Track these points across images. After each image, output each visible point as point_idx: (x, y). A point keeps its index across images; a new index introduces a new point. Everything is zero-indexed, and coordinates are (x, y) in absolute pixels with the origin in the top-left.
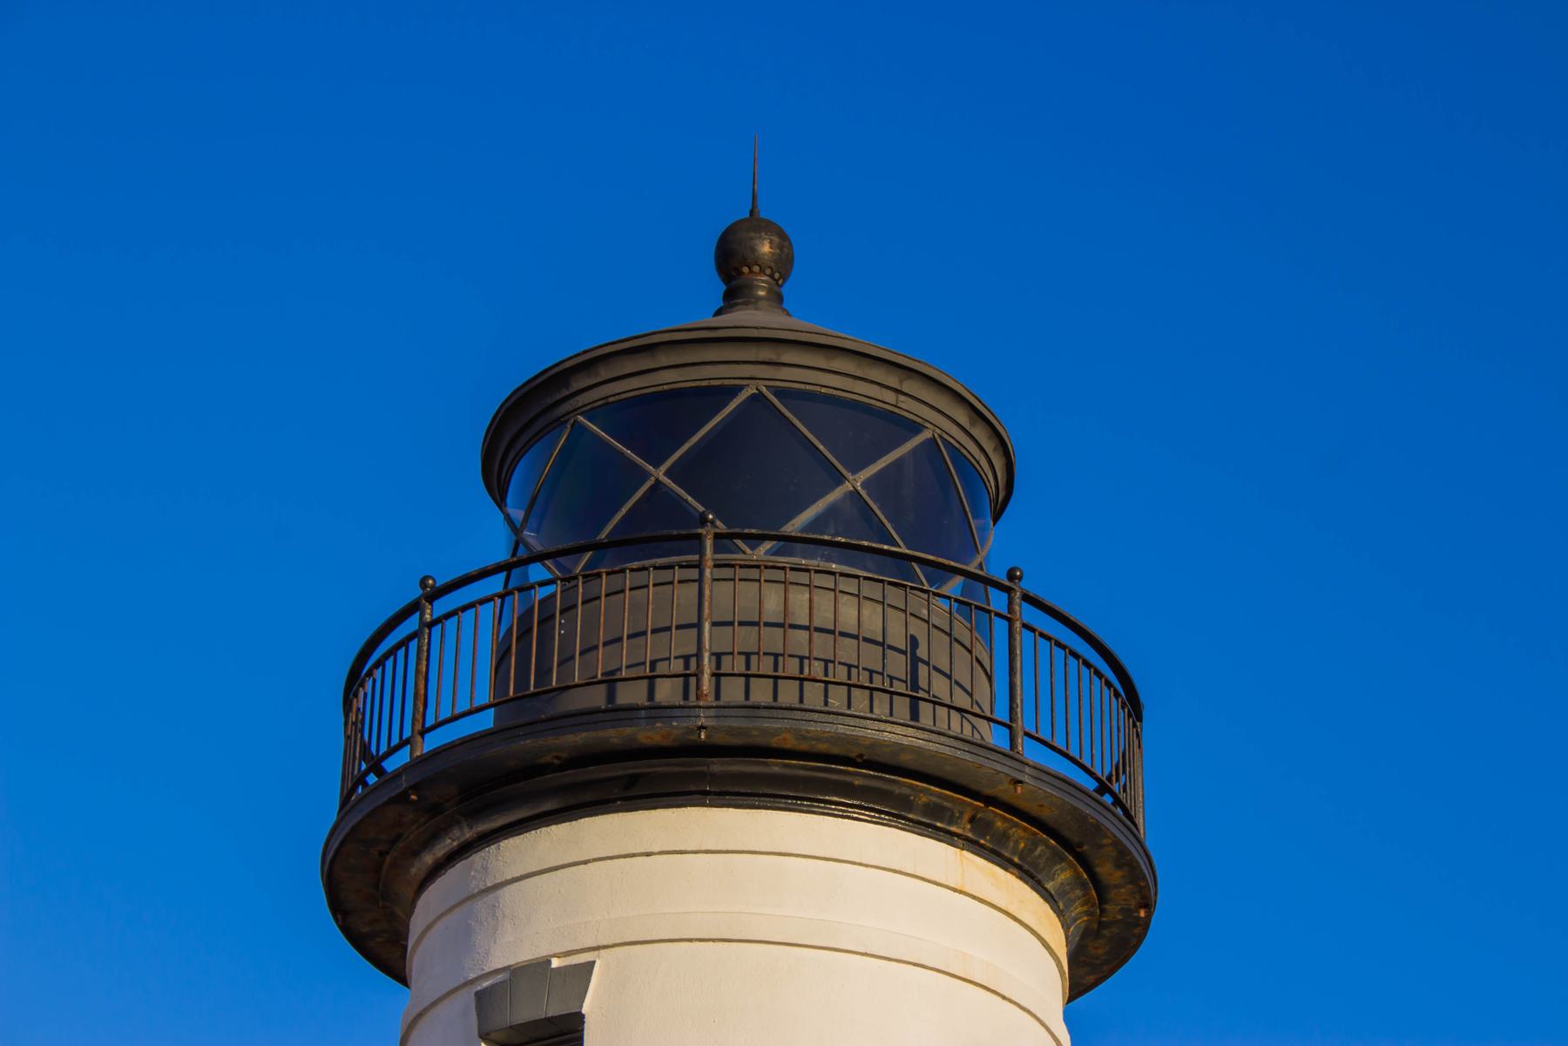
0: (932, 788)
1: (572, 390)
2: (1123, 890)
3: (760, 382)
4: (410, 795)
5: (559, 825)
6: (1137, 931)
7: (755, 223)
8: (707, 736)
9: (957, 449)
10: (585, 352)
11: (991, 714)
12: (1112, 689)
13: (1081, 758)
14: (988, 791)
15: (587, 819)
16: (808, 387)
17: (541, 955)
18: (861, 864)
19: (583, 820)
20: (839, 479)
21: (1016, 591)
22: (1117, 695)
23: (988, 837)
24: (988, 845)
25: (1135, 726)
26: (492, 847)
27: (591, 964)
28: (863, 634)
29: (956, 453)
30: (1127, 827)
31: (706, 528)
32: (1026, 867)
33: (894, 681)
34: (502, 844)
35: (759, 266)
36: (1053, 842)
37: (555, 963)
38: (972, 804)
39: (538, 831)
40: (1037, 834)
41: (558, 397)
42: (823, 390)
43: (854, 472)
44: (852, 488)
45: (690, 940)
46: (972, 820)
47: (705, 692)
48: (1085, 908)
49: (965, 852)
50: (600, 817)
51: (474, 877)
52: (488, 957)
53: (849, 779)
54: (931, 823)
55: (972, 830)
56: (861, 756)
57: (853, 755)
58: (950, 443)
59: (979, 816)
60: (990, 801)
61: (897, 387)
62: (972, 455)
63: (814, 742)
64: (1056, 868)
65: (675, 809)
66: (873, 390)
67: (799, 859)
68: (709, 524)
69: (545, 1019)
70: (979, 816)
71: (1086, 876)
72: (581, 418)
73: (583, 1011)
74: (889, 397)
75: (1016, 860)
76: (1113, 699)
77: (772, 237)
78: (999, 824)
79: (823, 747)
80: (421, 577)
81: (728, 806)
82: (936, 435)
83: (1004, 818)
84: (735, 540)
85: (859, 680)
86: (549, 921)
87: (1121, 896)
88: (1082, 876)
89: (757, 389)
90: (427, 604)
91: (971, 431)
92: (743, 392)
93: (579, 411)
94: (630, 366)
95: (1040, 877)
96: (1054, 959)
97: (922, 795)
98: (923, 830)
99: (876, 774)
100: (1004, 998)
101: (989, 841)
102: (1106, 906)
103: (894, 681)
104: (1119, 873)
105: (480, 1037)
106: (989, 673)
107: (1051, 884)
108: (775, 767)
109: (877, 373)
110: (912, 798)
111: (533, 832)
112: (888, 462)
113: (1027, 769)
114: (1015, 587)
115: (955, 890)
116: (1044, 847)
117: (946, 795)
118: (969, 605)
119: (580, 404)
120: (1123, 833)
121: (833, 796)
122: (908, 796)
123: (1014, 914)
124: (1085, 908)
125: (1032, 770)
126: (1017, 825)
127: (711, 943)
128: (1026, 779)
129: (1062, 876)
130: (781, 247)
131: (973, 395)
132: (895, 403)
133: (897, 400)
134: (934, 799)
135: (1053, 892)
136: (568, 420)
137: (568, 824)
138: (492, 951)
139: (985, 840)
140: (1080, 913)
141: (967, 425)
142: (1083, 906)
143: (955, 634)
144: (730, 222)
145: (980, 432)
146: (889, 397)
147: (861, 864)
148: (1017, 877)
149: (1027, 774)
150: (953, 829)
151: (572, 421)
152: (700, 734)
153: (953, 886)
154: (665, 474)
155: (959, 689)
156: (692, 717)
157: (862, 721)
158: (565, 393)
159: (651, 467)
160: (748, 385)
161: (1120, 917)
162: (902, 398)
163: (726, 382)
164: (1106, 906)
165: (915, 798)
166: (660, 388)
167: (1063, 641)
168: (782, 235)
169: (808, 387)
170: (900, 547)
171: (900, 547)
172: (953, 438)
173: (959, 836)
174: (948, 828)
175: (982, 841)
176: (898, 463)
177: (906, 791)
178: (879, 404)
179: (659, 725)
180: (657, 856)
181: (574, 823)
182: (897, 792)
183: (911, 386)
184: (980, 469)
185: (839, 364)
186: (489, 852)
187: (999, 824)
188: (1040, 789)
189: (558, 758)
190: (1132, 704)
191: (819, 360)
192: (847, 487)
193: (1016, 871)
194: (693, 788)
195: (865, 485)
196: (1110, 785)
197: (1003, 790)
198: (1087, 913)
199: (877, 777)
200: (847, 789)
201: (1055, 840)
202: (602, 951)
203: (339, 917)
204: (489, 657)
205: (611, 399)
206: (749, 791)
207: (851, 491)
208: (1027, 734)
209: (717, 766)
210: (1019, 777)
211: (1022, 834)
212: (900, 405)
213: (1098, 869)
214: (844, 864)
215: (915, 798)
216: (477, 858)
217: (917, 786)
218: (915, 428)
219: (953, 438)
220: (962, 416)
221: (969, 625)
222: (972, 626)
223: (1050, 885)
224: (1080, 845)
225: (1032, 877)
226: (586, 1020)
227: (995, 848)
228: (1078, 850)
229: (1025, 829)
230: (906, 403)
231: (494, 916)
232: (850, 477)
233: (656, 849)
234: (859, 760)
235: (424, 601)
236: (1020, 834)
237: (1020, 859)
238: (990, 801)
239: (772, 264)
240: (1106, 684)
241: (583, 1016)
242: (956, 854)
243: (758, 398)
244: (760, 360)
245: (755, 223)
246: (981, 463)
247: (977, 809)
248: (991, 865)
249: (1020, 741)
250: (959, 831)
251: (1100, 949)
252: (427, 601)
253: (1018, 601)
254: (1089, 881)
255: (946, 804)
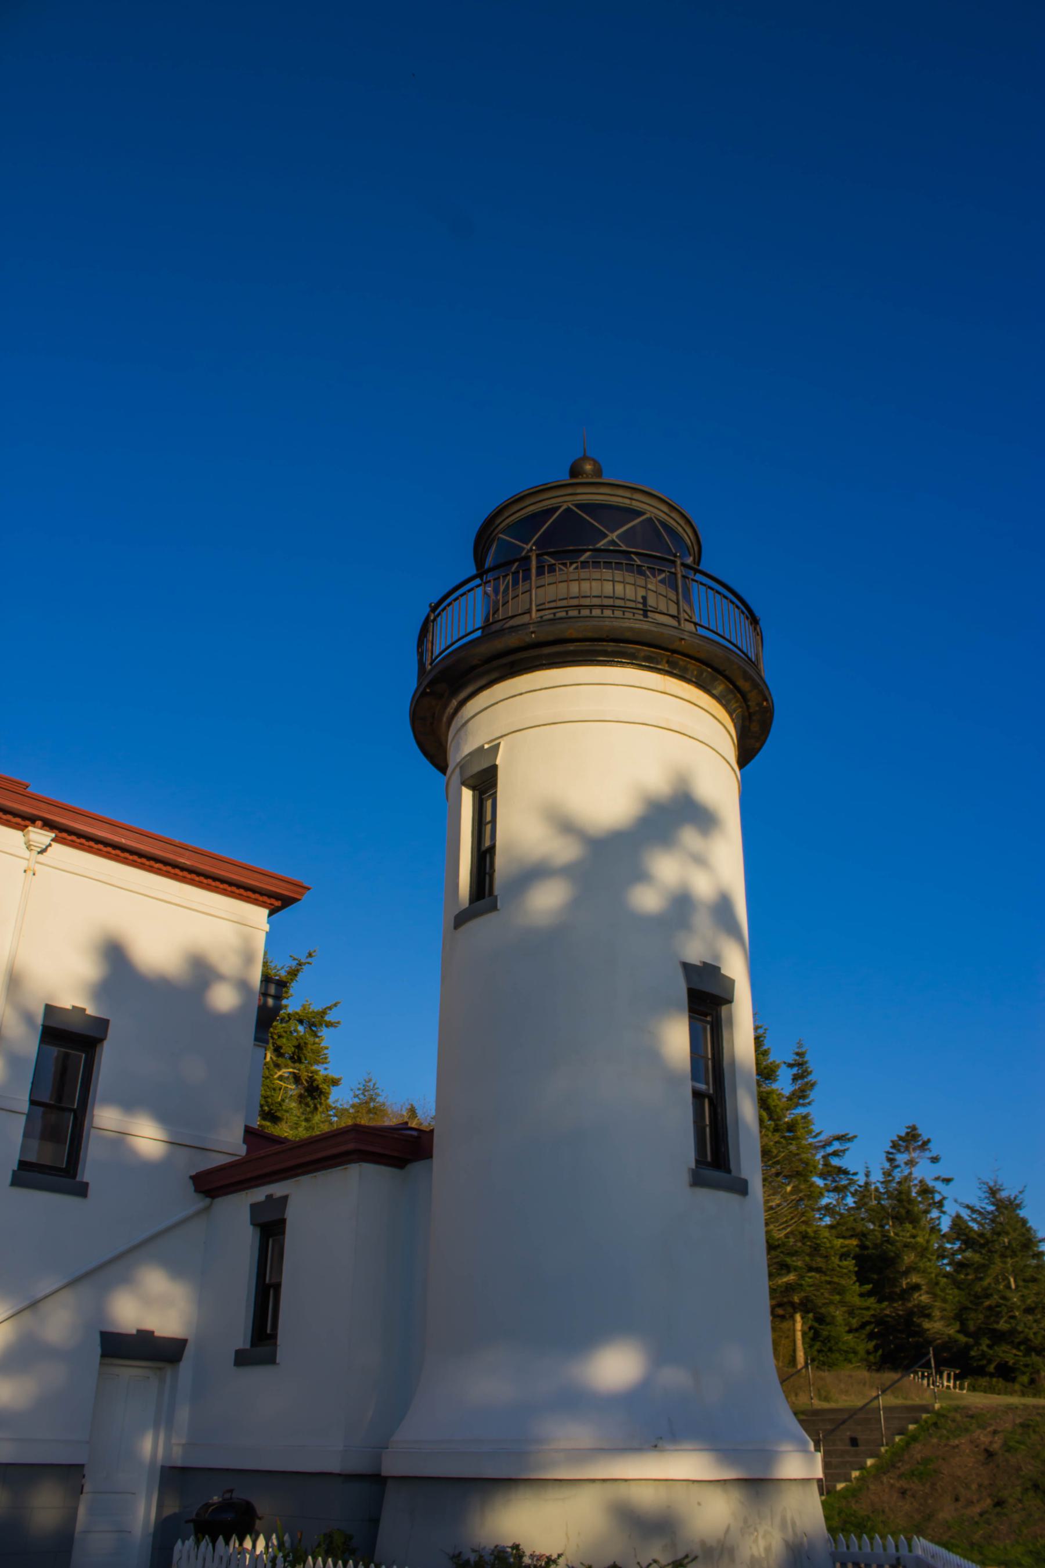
6: (768, 714)
8: (535, 636)
14: (671, 647)
20: (605, 536)
22: (747, 618)
25: (755, 629)
27: (499, 744)
28: (616, 595)
29: (665, 525)
32: (700, 683)
37: (486, 746)
48: (737, 704)
53: (605, 648)
54: (650, 664)
55: (669, 667)
56: (607, 636)
66: (620, 499)
72: (500, 535)
74: (628, 501)
75: (694, 680)
83: (682, 659)
87: (753, 696)
94: (516, 508)
95: (709, 688)
100: (690, 737)
108: (571, 647)
109: (620, 492)
113: (686, 633)
118: (654, 569)
129: (719, 689)
130: (594, 465)
146: (628, 501)
150: (659, 667)
158: (494, 527)
162: (634, 502)
167: (704, 582)
176: (633, 527)
183: (636, 496)
190: (754, 621)
195: (618, 537)
197: (676, 645)
198: (740, 707)
209: (547, 650)
210: (682, 637)
216: (460, 714)
218: (640, 513)
220: (665, 508)
222: (678, 599)
223: (714, 692)
229: (694, 664)
230: (634, 503)
236: (693, 667)
237: (696, 678)
243: (568, 510)
245: (585, 458)
247: (667, 656)
251: (755, 727)
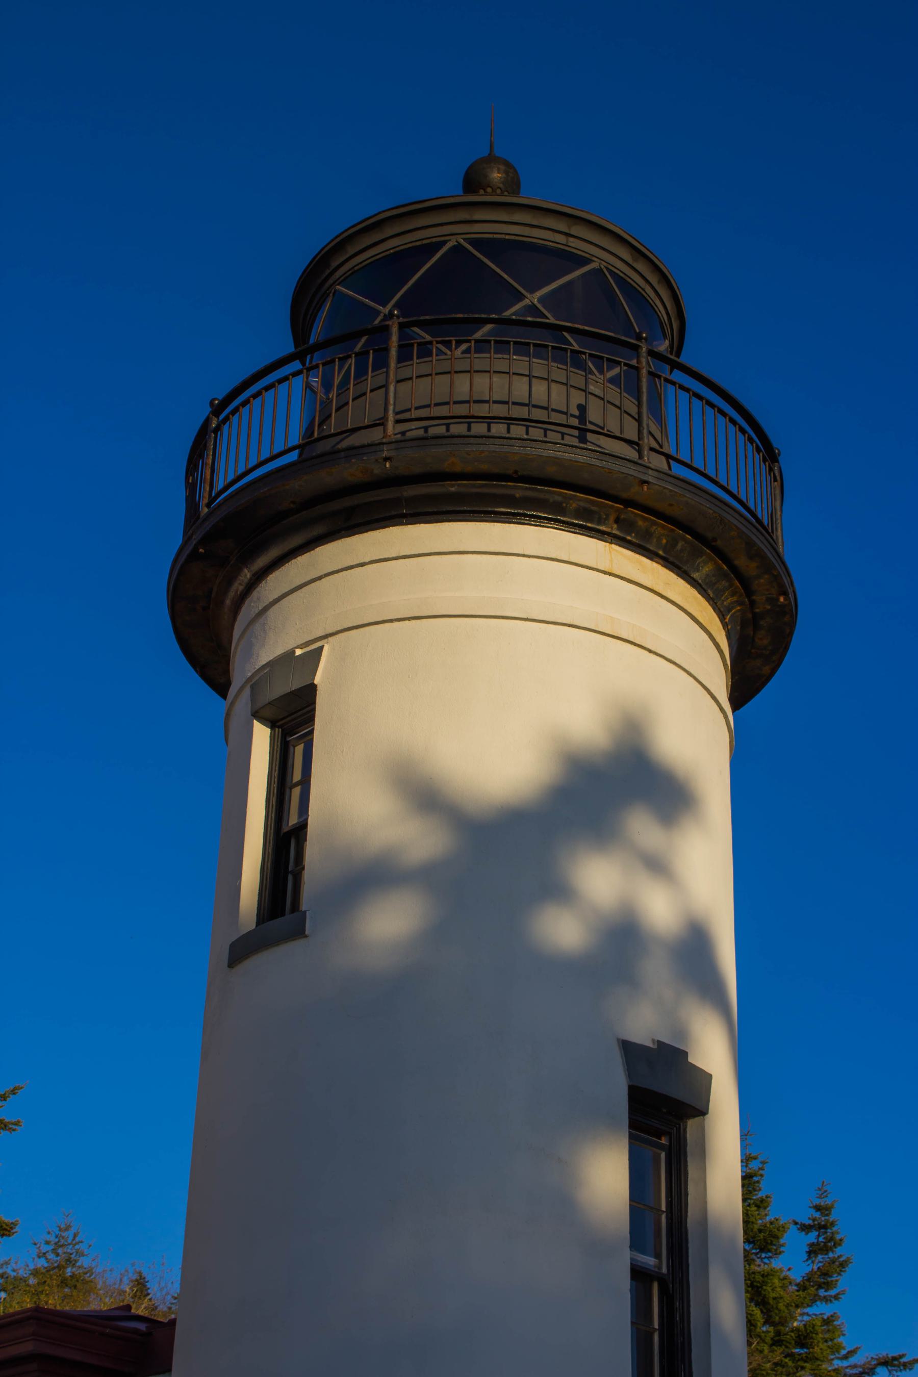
0: (578, 494)
1: (332, 268)
2: (762, 581)
3: (458, 236)
4: (199, 550)
5: (303, 556)
6: (787, 619)
7: (491, 159)
9: (622, 278)
10: (336, 237)
11: (621, 434)
12: (737, 426)
13: (705, 470)
14: (624, 495)
15: (320, 547)
16: (495, 236)
17: (289, 648)
18: (524, 556)
19: (318, 549)
21: (642, 348)
23: (633, 535)
24: (634, 540)
26: (263, 582)
29: (622, 282)
30: (767, 540)
31: (392, 321)
32: (671, 559)
33: (565, 436)
34: (268, 578)
35: (491, 187)
36: (689, 537)
37: (298, 652)
38: (613, 506)
39: (290, 563)
40: (673, 530)
41: (324, 276)
42: (507, 237)
43: (532, 292)
44: (530, 303)
45: (391, 621)
46: (617, 521)
47: (389, 434)
48: (735, 598)
49: (613, 546)
50: (329, 544)
51: (253, 606)
52: (258, 659)
55: (618, 529)
56: (516, 472)
57: (510, 472)
58: (614, 272)
59: (622, 517)
60: (629, 503)
61: (567, 231)
62: (637, 284)
63: (476, 464)
64: (698, 562)
65: (381, 530)
67: (475, 556)
68: (395, 317)
69: (291, 692)
70: (622, 517)
71: (726, 568)
72: (338, 287)
73: (316, 682)
74: (561, 239)
75: (661, 553)
76: (756, 453)
77: (500, 166)
78: (640, 523)
79: (484, 467)
80: (209, 401)
81: (420, 523)
82: (602, 267)
83: (643, 517)
84: (412, 328)
85: (509, 415)
86: (296, 624)
88: (723, 568)
89: (457, 242)
90: (214, 417)
91: (633, 265)
92: (446, 245)
93: (337, 282)
95: (685, 568)
96: (683, 611)
97: (571, 502)
98: (584, 531)
99: (530, 486)
100: (650, 651)
101: (634, 537)
102: (754, 597)
103: (565, 436)
104: (753, 565)
105: (252, 715)
106: (661, 443)
107: (697, 574)
108: (453, 487)
109: (549, 222)
110: (564, 505)
111: (287, 565)
112: (559, 284)
113: (650, 472)
114: (640, 344)
115: (604, 572)
116: (684, 543)
117: (591, 500)
119: (337, 277)
120: (742, 524)
121: (500, 508)
122: (561, 503)
123: (660, 592)
124: (735, 598)
125: (654, 472)
126: (654, 523)
127: (407, 622)
128: (651, 480)
129: (705, 570)
130: (507, 173)
131: (630, 235)
132: (565, 243)
133: (567, 241)
134: (582, 504)
135: (700, 581)
136: (330, 292)
137: (308, 553)
138: (260, 653)
139: (631, 536)
140: (732, 603)
141: (630, 261)
142: (732, 596)
143: (624, 408)
144: (469, 164)
145: (641, 266)
146: (561, 239)
147: (524, 556)
148: (662, 566)
149: (650, 475)
151: (333, 291)
152: (385, 464)
153: (603, 569)
154: (384, 306)
155: (598, 423)
156: (378, 451)
157: (509, 440)
158: (328, 272)
159: (381, 307)
160: (450, 240)
161: (769, 607)
162: (571, 239)
163: (434, 240)
164: (754, 597)
165: (567, 505)
166: (388, 253)
168: (507, 164)
169: (495, 236)
170: (548, 319)
171: (548, 319)
172: (618, 269)
173: (609, 534)
174: (598, 527)
175: (629, 538)
176: (570, 283)
177: (559, 499)
178: (551, 244)
179: (353, 460)
180: (369, 566)
181: (312, 552)
182: (551, 500)
183: (577, 230)
184: (645, 295)
185: (518, 217)
186: (261, 586)
187: (640, 523)
188: (665, 488)
189: (293, 502)
190: (770, 455)
191: (503, 216)
192: (526, 302)
193: (661, 561)
194: (393, 513)
195: (540, 300)
196: (547, 321)
197: (634, 492)
199: (527, 488)
200: (510, 501)
201: (691, 536)
202: (330, 639)
203: (198, 669)
204: (241, 440)
205: (356, 268)
206: (435, 510)
207: (529, 306)
208: (652, 449)
210: (645, 478)
211: (662, 532)
212: (570, 244)
213: (736, 562)
214: (510, 557)
215: (567, 505)
216: (255, 594)
217: (566, 493)
218: (583, 261)
219: (618, 269)
220: (625, 254)
221: (619, 391)
223: (696, 575)
224: (715, 540)
225: (679, 568)
226: (318, 688)
227: (640, 543)
228: (713, 544)
229: (663, 527)
230: (573, 242)
231: (264, 630)
232: (528, 295)
233: (367, 560)
234: (514, 476)
235: (211, 416)
236: (660, 529)
237: (664, 551)
238: (629, 503)
239: (501, 186)
240: (748, 440)
241: (316, 686)
242: (606, 546)
243: (458, 248)
244: (458, 220)
245: (491, 159)
246: (646, 290)
247: (618, 510)
248: (637, 556)
249: (646, 453)
250: (609, 530)
251: (763, 640)
252: (213, 415)
253: (645, 355)
254: (729, 572)
255: (593, 508)
